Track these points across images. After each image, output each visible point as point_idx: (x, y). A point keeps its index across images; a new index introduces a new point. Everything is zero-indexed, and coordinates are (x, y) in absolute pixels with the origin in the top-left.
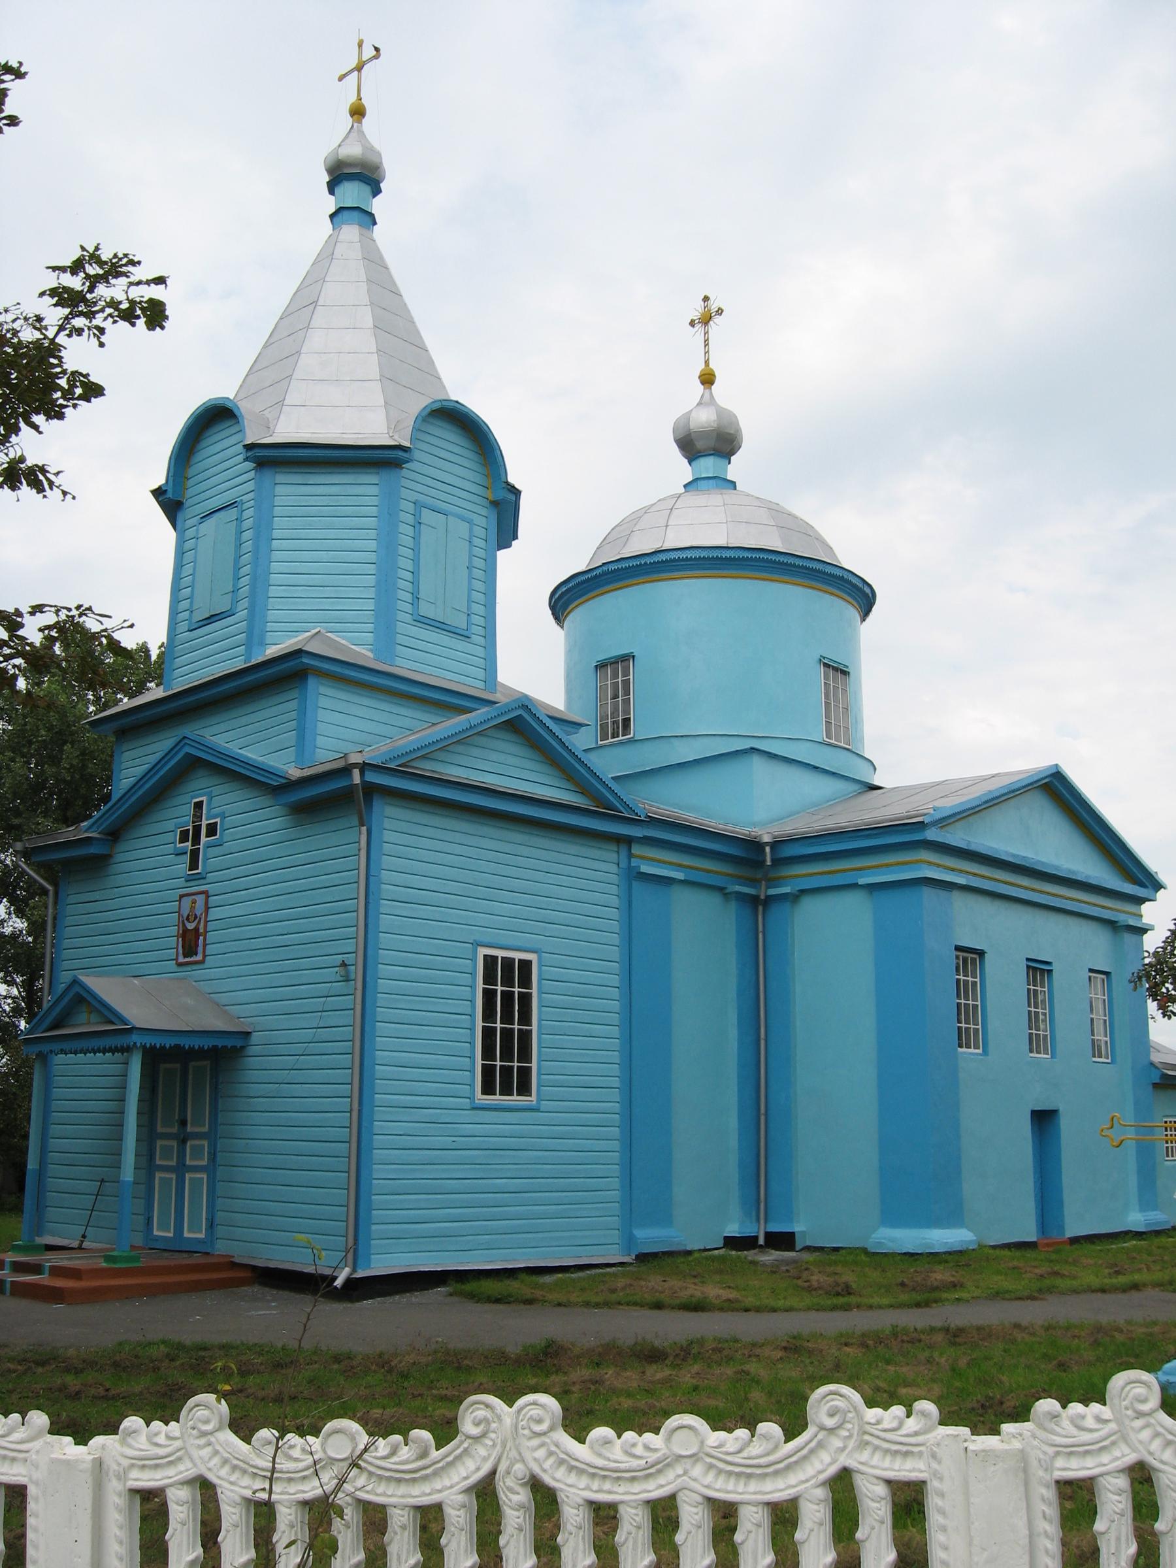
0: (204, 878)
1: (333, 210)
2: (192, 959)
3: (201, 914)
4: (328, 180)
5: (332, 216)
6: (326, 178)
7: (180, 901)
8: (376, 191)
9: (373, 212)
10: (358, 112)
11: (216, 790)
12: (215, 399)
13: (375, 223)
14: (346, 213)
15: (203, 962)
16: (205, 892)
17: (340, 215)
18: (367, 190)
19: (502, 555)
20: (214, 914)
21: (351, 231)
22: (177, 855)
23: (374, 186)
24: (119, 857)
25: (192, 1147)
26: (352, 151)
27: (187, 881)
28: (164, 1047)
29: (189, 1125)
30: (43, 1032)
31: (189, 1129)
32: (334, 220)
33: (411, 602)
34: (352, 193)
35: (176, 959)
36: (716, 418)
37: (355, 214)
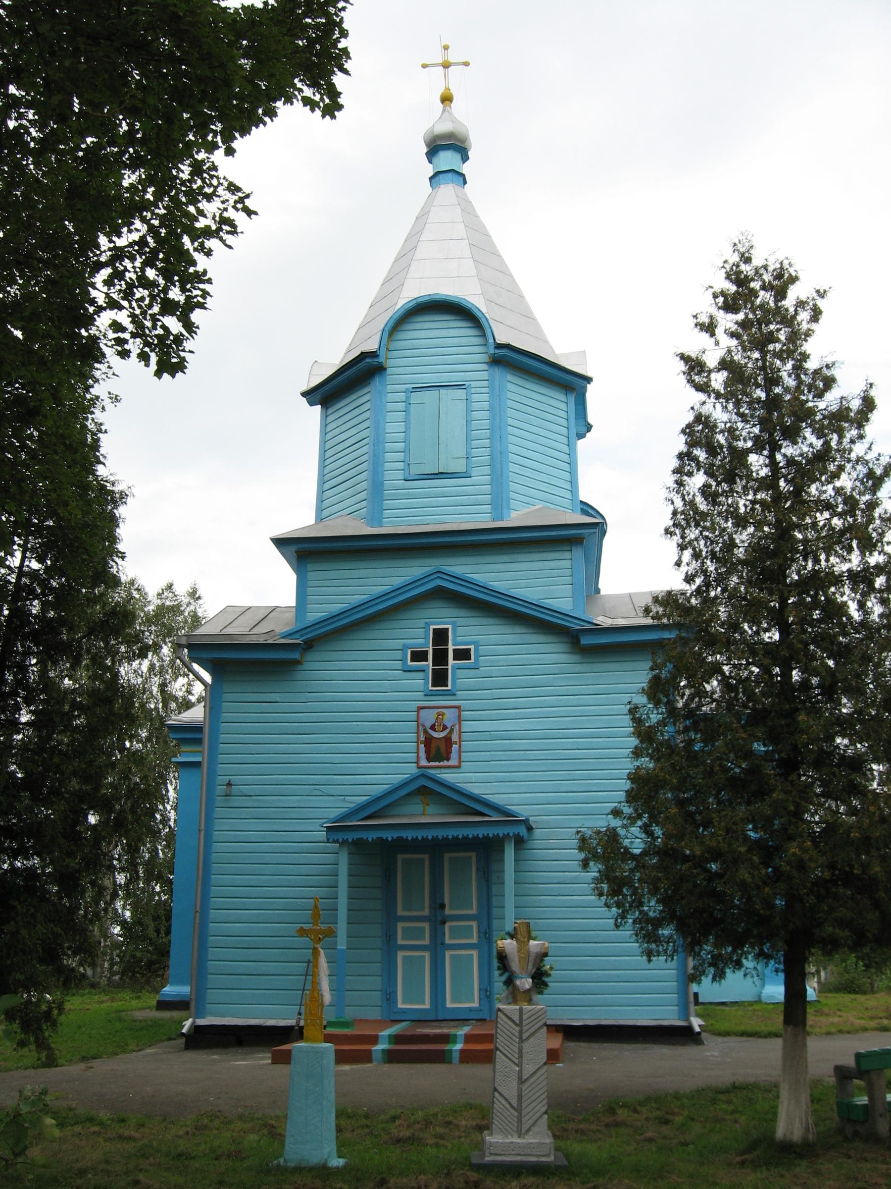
0: (455, 695)
1: (432, 174)
2: (442, 764)
3: (454, 726)
4: (426, 151)
5: (431, 179)
6: (425, 150)
7: (418, 711)
8: (465, 158)
9: (464, 173)
10: (447, 99)
11: (460, 621)
12: (447, 295)
13: (465, 182)
14: (441, 176)
15: (459, 767)
16: (458, 707)
17: (437, 179)
18: (457, 157)
19: (580, 443)
20: (466, 726)
21: (447, 190)
22: (404, 671)
23: (463, 152)
24: (307, 665)
25: (450, 927)
26: (444, 128)
27: (425, 695)
28: (427, 839)
29: (447, 908)
30: (363, 819)
31: (447, 911)
32: (433, 181)
33: (569, 470)
34: (447, 160)
35: (417, 763)
36: (319, 406)
37: (450, 175)
